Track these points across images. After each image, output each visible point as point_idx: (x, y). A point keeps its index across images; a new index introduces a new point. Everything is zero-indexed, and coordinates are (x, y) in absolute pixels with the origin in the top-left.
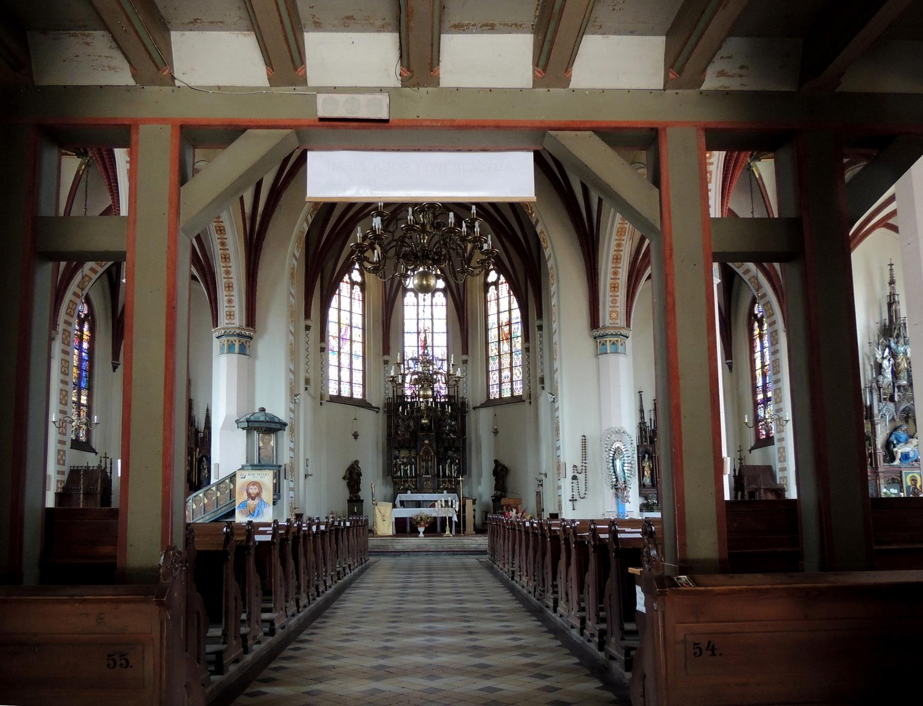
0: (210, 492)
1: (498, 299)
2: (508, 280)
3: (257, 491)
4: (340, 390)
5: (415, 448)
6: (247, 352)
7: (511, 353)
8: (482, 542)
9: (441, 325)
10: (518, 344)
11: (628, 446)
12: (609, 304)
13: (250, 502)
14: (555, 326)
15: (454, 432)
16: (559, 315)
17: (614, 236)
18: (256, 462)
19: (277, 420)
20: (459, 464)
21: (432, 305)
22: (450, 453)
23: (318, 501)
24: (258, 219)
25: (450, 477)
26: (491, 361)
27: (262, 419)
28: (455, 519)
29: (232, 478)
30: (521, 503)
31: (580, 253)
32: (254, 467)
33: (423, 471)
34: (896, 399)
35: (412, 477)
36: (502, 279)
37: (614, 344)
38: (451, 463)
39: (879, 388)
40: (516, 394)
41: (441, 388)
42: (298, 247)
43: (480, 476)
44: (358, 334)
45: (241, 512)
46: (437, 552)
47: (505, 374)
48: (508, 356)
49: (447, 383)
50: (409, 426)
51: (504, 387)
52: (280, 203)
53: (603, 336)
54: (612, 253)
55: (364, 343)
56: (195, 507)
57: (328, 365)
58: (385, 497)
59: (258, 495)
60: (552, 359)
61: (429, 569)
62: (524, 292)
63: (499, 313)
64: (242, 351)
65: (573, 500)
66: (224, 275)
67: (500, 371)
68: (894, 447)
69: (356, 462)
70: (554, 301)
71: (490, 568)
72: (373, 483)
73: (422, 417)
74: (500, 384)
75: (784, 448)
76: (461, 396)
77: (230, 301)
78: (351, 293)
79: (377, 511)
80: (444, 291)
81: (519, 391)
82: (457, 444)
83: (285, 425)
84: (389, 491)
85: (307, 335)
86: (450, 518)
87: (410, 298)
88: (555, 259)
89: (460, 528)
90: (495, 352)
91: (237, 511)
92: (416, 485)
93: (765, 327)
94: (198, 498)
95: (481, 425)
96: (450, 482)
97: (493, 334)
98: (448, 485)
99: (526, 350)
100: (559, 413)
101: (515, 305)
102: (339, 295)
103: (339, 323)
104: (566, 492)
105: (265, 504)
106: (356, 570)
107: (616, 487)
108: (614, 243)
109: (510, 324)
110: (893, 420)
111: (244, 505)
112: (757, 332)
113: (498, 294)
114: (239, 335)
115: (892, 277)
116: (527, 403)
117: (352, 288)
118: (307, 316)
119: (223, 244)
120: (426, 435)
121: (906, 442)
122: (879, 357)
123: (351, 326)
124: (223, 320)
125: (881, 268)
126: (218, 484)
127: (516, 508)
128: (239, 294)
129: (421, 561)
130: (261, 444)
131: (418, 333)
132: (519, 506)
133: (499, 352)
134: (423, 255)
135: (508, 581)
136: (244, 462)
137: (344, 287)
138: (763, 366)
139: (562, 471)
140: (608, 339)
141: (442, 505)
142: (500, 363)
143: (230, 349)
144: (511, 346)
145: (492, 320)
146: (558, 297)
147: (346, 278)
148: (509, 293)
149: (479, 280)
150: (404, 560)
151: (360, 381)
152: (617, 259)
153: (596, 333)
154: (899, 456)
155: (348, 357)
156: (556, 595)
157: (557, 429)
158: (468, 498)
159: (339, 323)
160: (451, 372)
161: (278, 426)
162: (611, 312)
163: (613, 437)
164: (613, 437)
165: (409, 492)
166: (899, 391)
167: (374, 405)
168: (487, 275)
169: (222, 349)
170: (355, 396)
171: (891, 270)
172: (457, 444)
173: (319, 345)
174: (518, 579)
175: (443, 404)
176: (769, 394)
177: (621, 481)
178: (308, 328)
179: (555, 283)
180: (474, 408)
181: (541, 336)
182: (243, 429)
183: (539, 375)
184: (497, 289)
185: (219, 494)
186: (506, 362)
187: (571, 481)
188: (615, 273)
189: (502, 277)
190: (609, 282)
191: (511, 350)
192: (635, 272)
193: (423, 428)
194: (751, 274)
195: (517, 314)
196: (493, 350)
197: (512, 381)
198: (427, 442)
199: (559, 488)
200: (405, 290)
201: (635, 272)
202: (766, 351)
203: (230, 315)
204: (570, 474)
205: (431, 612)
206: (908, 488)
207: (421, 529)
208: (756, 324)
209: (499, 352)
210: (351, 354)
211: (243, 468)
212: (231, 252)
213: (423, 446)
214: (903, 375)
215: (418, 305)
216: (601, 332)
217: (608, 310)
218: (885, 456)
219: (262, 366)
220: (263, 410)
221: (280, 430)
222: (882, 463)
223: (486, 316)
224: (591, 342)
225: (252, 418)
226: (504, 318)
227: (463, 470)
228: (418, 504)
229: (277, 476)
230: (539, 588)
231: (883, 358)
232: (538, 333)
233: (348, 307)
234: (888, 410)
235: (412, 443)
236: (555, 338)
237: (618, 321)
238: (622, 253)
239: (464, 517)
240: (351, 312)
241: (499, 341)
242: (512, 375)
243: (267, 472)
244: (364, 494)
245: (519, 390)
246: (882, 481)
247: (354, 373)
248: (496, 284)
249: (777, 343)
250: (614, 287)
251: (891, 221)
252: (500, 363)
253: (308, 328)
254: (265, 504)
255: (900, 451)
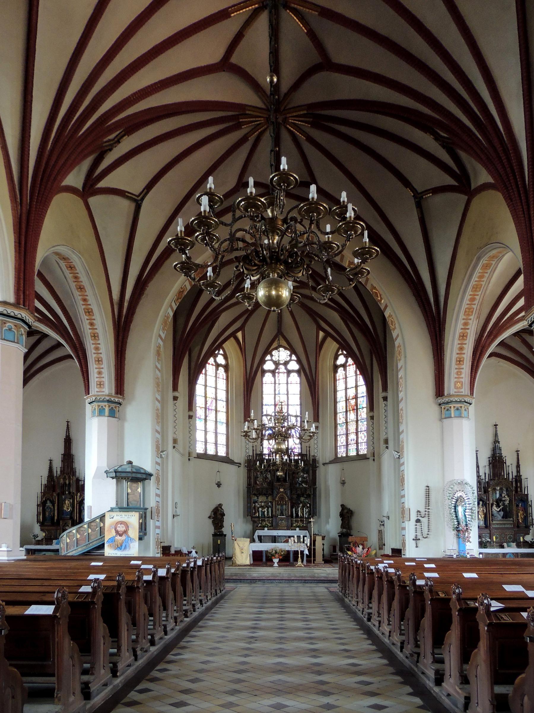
0: (82, 529)
1: (346, 378)
3: (124, 528)
4: (206, 449)
5: (272, 494)
6: (117, 415)
7: (357, 421)
8: (332, 571)
9: (295, 400)
10: (363, 413)
13: (118, 538)
14: (401, 395)
15: (306, 483)
16: (406, 386)
17: (462, 316)
18: (125, 505)
19: (142, 471)
20: (310, 507)
21: (287, 383)
22: (302, 499)
23: (188, 535)
24: (126, 304)
25: (302, 517)
27: (129, 470)
28: (306, 552)
29: (102, 518)
32: (122, 509)
33: (278, 512)
35: (269, 517)
36: (350, 361)
37: (458, 409)
38: (303, 507)
40: (361, 453)
41: (294, 444)
42: (163, 329)
43: (328, 516)
44: (222, 406)
45: (110, 546)
46: (290, 581)
47: (351, 435)
48: (355, 423)
49: (300, 438)
50: (266, 478)
51: (350, 447)
52: (146, 292)
53: (447, 403)
54: (459, 331)
55: (227, 412)
56: (68, 541)
57: (195, 429)
58: (245, 532)
59: (125, 532)
60: (397, 422)
61: (282, 600)
63: (346, 389)
64: (112, 414)
65: (416, 539)
66: (94, 351)
67: (347, 435)
69: (220, 505)
71: (341, 601)
72: (235, 522)
73: (278, 470)
74: (347, 445)
76: (312, 454)
77: (100, 373)
78: (216, 373)
79: (236, 545)
80: (298, 372)
81: (363, 450)
82: (308, 492)
83: (151, 475)
84: (249, 527)
85: (175, 404)
86: (302, 552)
87: (268, 378)
89: (311, 558)
91: (106, 545)
92: (272, 523)
94: (71, 534)
95: (329, 478)
96: (302, 521)
97: (341, 406)
98: (300, 524)
100: (405, 467)
101: (361, 381)
102: (206, 374)
103: (206, 397)
105: (132, 540)
106: (209, 603)
107: (457, 529)
108: (461, 322)
109: (356, 397)
111: (112, 540)
114: (108, 401)
117: (217, 369)
118: (175, 388)
119: (92, 324)
120: (281, 487)
123: (216, 399)
124: (94, 389)
126: (90, 523)
127: (363, 545)
128: (109, 367)
129: (275, 589)
130: (129, 491)
131: (275, 405)
132: (365, 543)
133: (346, 420)
134: (271, 258)
135: (363, 621)
136: (114, 505)
137: (210, 368)
139: (406, 515)
140: (452, 406)
141: (294, 541)
142: (347, 429)
143: (101, 412)
145: (341, 395)
147: (211, 360)
149: (329, 363)
150: (259, 588)
151: (224, 442)
152: (463, 336)
153: (440, 400)
155: (214, 423)
157: (402, 481)
158: (318, 535)
159: (206, 397)
160: (306, 428)
161: (144, 476)
162: (456, 383)
164: (456, 488)
165: (266, 529)
167: (236, 461)
169: (93, 412)
170: (219, 454)
172: (308, 492)
173: (187, 414)
175: (296, 461)
177: (463, 524)
178: (175, 398)
179: (403, 359)
180: (324, 464)
181: (386, 405)
182: (113, 478)
183: (383, 437)
184: (345, 370)
185: (90, 531)
186: (352, 428)
187: (415, 523)
188: (461, 349)
190: (455, 356)
192: (480, 348)
193: (278, 479)
195: (363, 390)
196: (341, 418)
197: (357, 443)
198: (282, 490)
199: (404, 529)
200: (264, 372)
201: (480, 348)
203: (100, 385)
204: (414, 517)
205: (280, 672)
207: (276, 561)
209: (346, 420)
210: (216, 422)
211: (112, 510)
212: (100, 331)
213: (278, 493)
215: (275, 383)
216: (446, 400)
217: (453, 380)
219: (129, 427)
220: (130, 463)
221: (146, 479)
223: (335, 391)
224: (436, 408)
225: (120, 470)
226: (351, 393)
227: (313, 512)
228: (274, 539)
229: (143, 517)
232: (382, 403)
233: (213, 384)
235: (269, 490)
236: (402, 405)
238: (468, 331)
239: (314, 549)
240: (216, 388)
241: (346, 411)
242: (357, 438)
243: (134, 513)
244: (226, 530)
247: (219, 436)
248: (344, 366)
252: (347, 429)
253: (175, 398)
254: (132, 540)
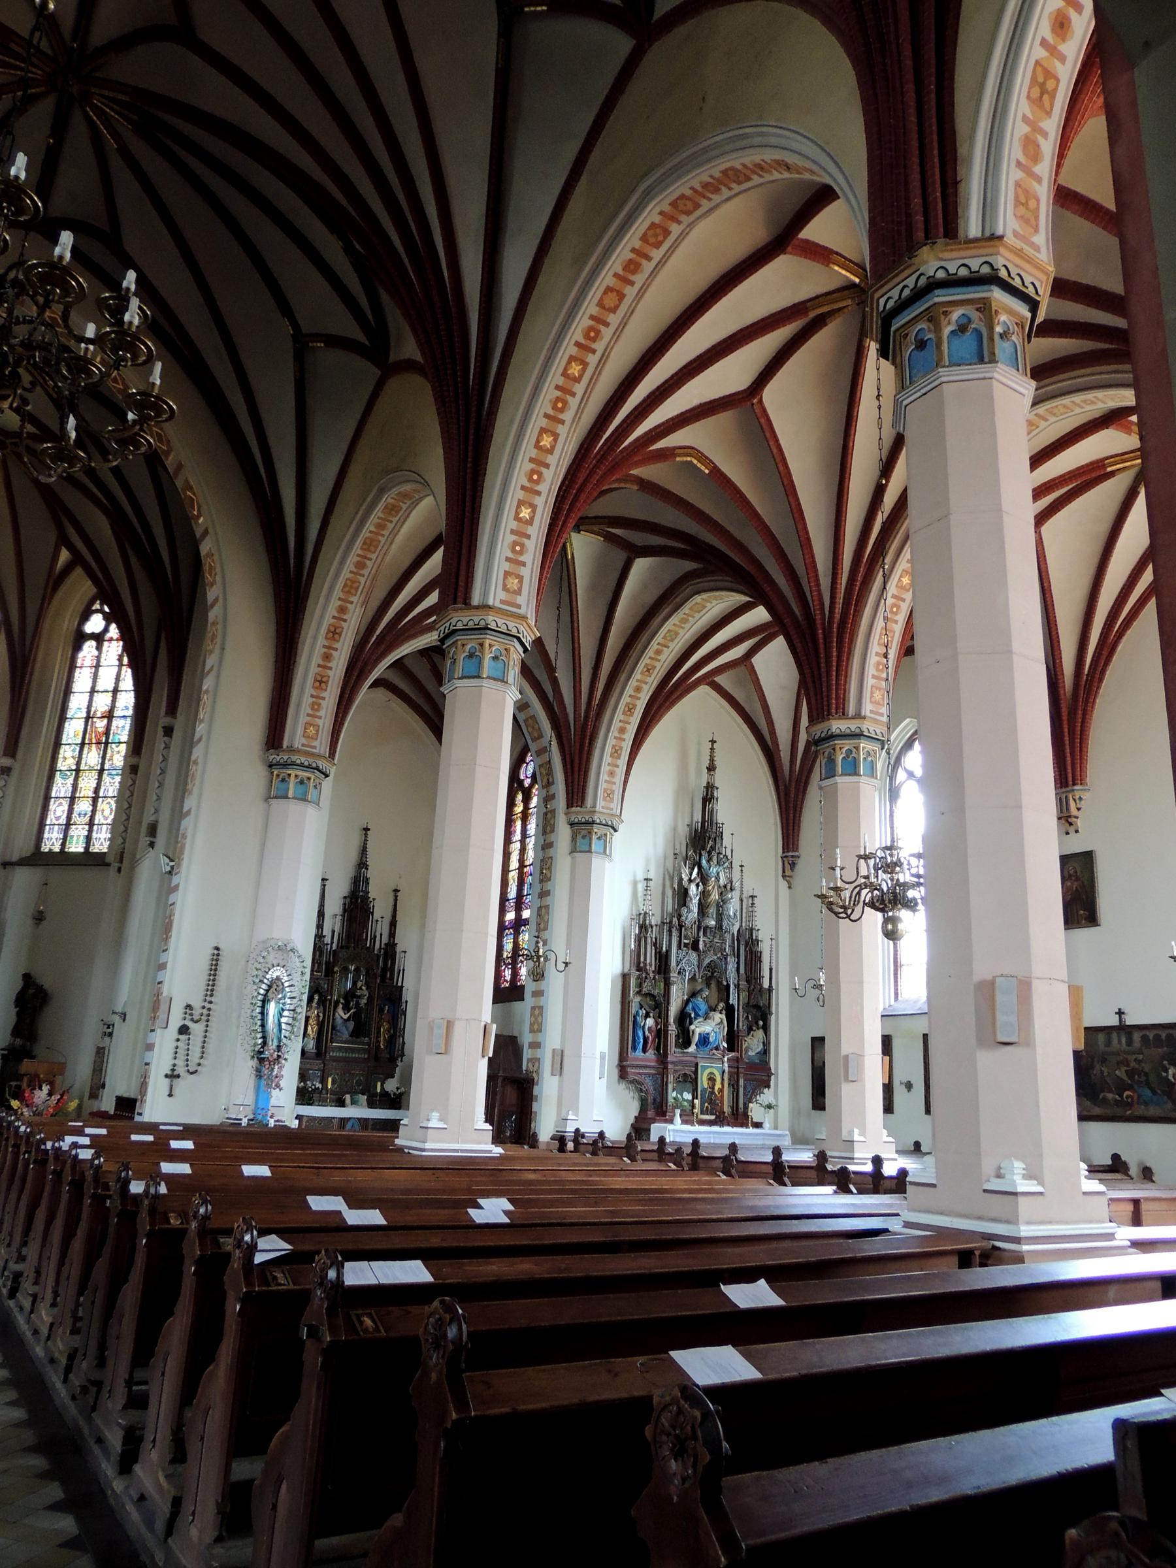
1: (97, 666)
2: (125, 636)
7: (101, 772)
10: (118, 756)
11: (297, 977)
12: (305, 708)
14: (201, 729)
26: (58, 779)
30: (62, 1073)
31: (272, 609)
34: (701, 946)
36: (114, 631)
37: (302, 782)
39: (681, 926)
48: (95, 775)
51: (73, 831)
53: (285, 765)
54: (328, 620)
62: (149, 661)
63: (93, 691)
65: (173, 1076)
68: (691, 1023)
70: (208, 683)
74: (68, 825)
75: (541, 1008)
88: (225, 608)
90: (71, 763)
93: (534, 802)
97: (73, 729)
99: (132, 769)
101: (128, 682)
104: (161, 1061)
107: (260, 1057)
108: (334, 603)
109: (109, 716)
110: (693, 979)
112: (519, 808)
113: (98, 658)
115: (712, 760)
116: (112, 872)
121: (706, 1017)
122: (685, 878)
125: (699, 744)
127: (51, 1084)
132: (58, 1079)
133: (78, 764)
138: (522, 865)
139: (162, 1015)
140: (293, 773)
142: (75, 786)
144: (104, 758)
145: (78, 703)
146: (218, 676)
148: (120, 659)
149: (67, 623)
152: (334, 633)
153: (274, 757)
154: (696, 1039)
156: (135, 1415)
157: (167, 928)
163: (271, 958)
166: (705, 934)
168: (85, 616)
171: (712, 749)
174: (27, 1303)
176: (526, 914)
177: (272, 1045)
179: (217, 651)
181: (167, 747)
183: (148, 818)
184: (99, 648)
186: (87, 784)
187: (176, 1036)
188: (327, 657)
189: (113, 627)
191: (103, 764)
194: (530, 712)
195: (127, 701)
196: (66, 758)
197: (91, 824)
199: (150, 1047)
201: (359, 666)
202: (531, 843)
204: (176, 1021)
206: (704, 1090)
208: (520, 797)
209: (78, 764)
214: (712, 910)
217: (303, 719)
218: (677, 1036)
222: (673, 1049)
223: (68, 692)
224: (261, 772)
226: (102, 703)
230: (84, 1365)
231: (690, 881)
232: (161, 740)
234: (689, 963)
236: (197, 752)
237: (316, 743)
241: (83, 744)
242: (94, 812)
245: (102, 842)
246: (671, 1078)
248: (99, 638)
249: (552, 831)
250: (321, 682)
251: (718, 679)
252: (75, 786)
255: (698, 1031)
